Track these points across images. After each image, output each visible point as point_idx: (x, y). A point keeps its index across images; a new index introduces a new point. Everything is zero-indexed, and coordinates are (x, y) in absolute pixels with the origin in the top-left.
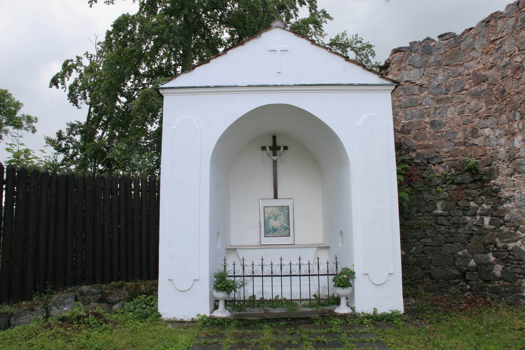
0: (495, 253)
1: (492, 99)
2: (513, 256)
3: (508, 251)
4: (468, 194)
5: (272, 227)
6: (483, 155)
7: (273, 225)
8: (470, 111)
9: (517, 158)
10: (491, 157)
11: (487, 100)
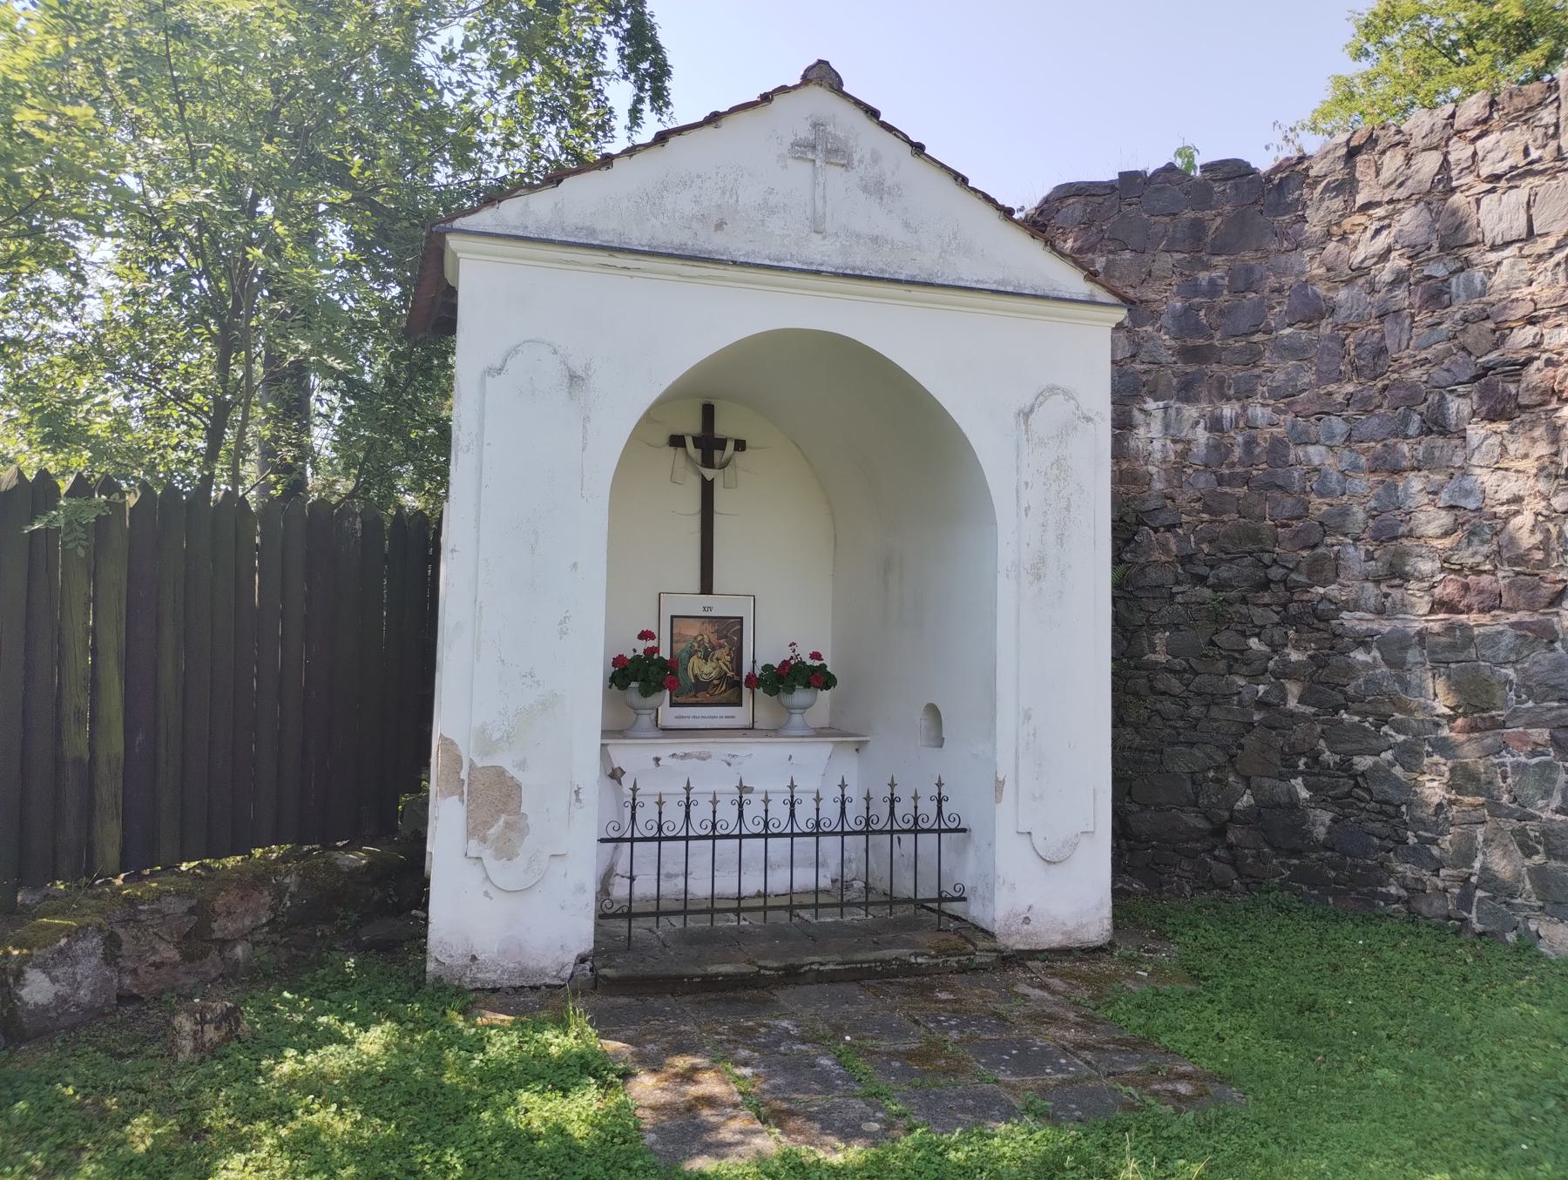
0: (1312, 779)
1: (1343, 368)
2: (1369, 791)
3: (1354, 777)
4: (1249, 619)
5: (696, 677)
6: (1299, 518)
7: (697, 671)
8: (1270, 391)
9: (1403, 536)
10: (1321, 524)
11: (1324, 368)
